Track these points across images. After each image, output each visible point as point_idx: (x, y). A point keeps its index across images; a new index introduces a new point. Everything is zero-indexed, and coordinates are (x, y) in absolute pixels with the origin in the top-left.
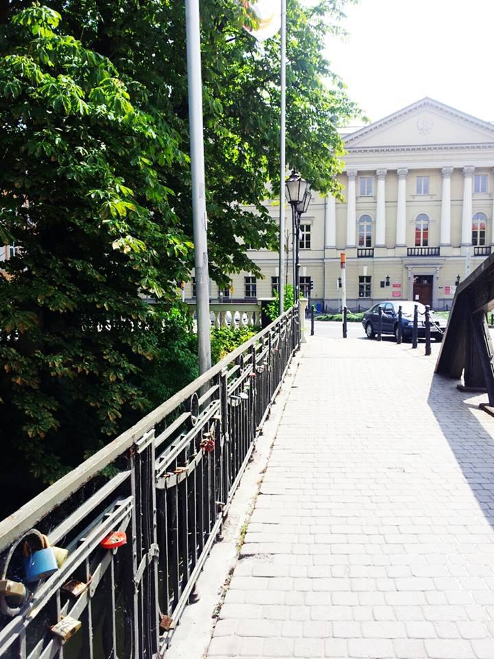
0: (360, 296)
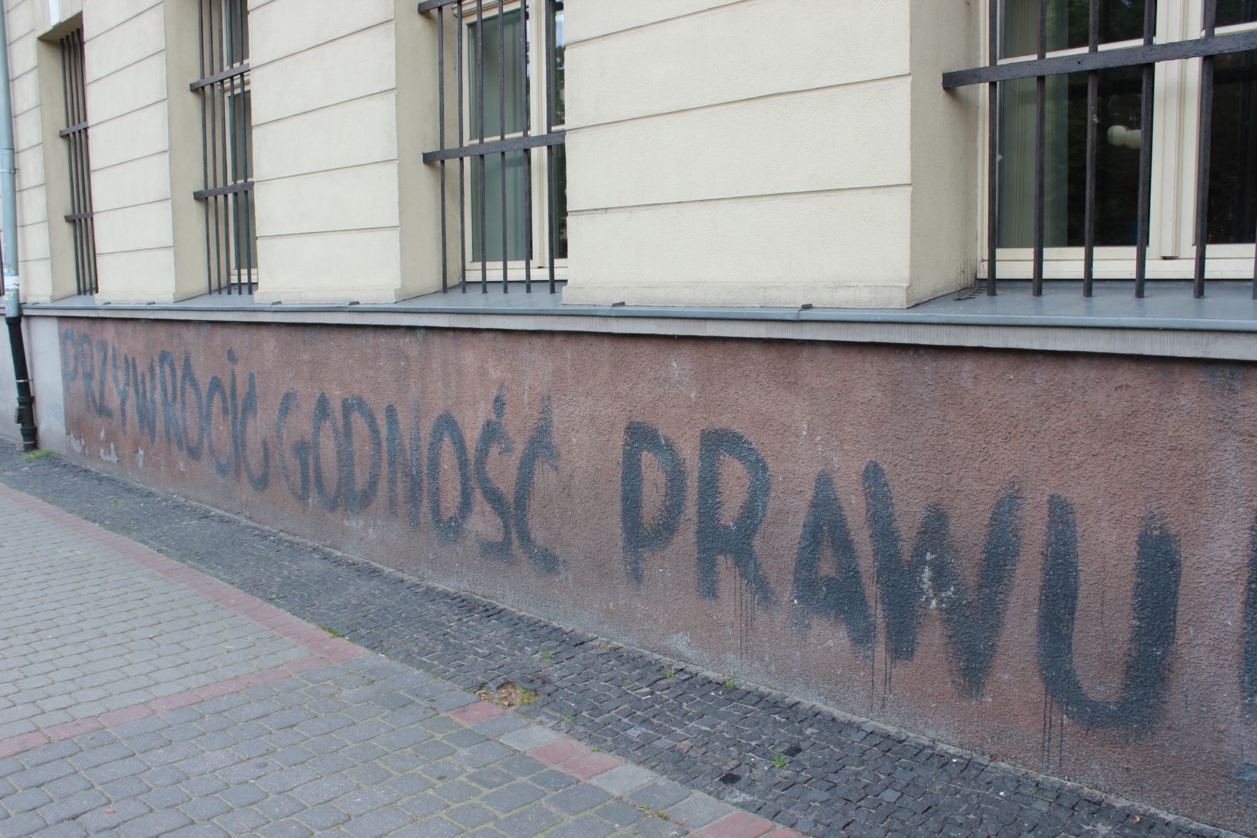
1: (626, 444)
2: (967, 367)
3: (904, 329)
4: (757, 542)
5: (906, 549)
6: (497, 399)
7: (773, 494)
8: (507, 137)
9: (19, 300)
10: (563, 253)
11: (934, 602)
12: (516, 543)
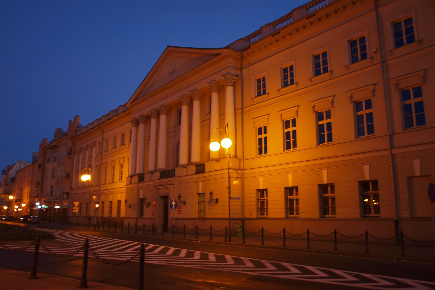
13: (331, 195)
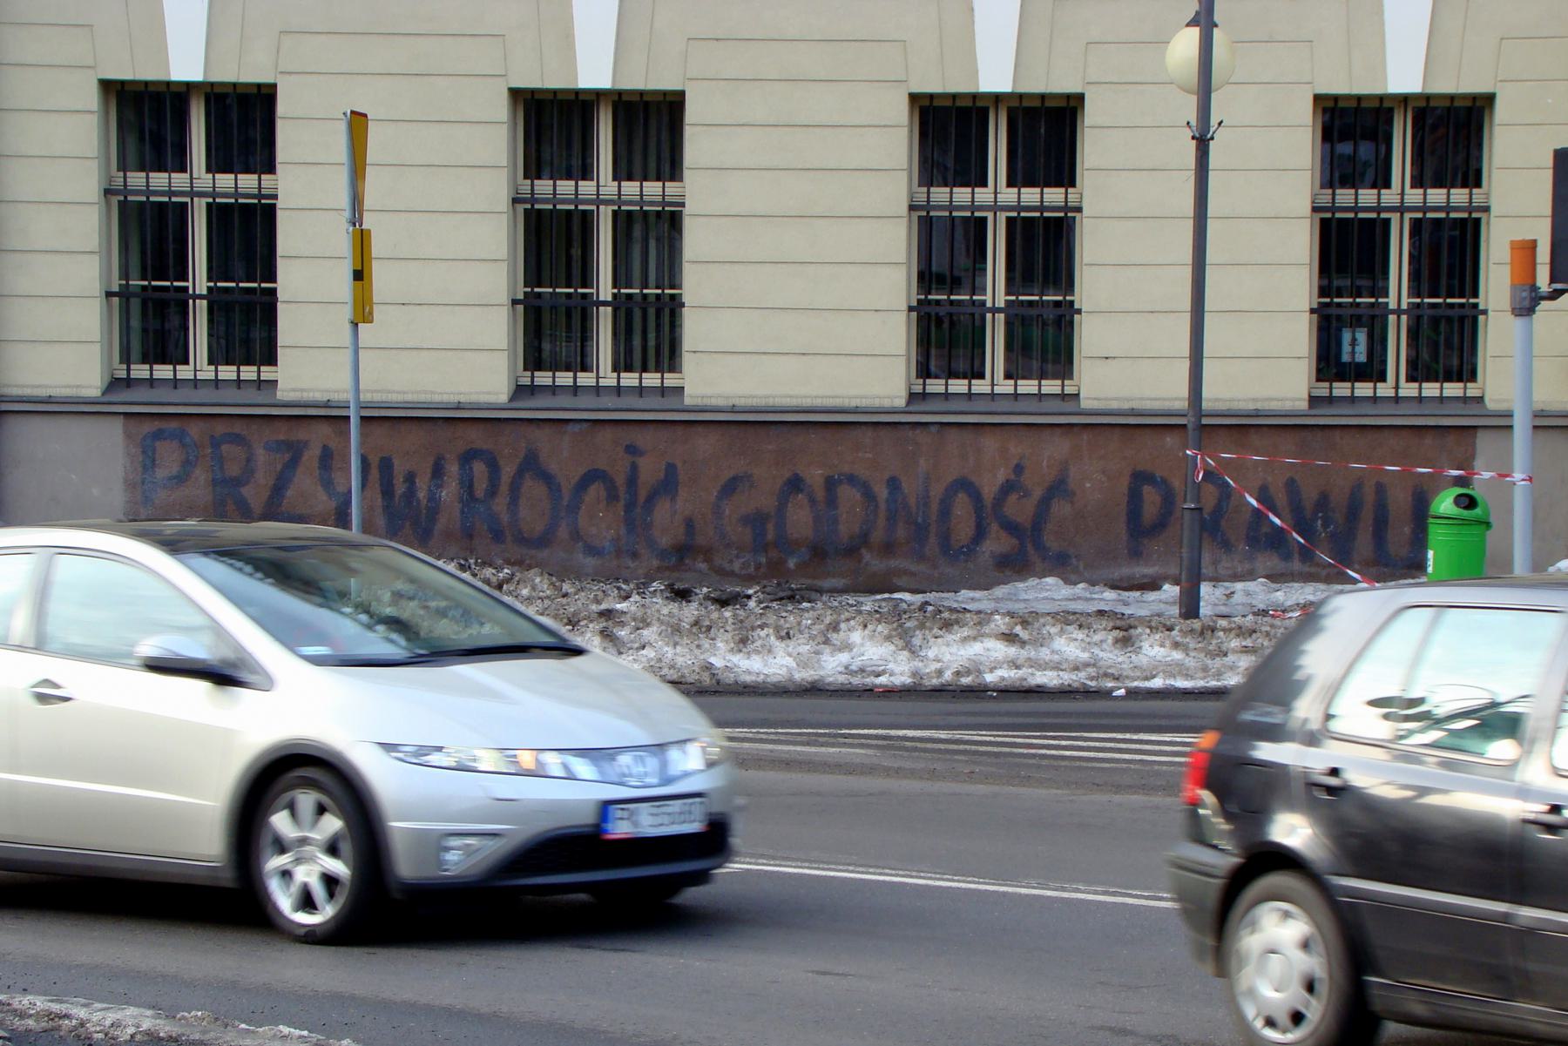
0: (1329, 364)
1: (1130, 483)
2: (1337, 433)
3: (1332, 418)
4: (1223, 523)
5: (1308, 513)
6: (1017, 466)
7: (1233, 498)
8: (638, 208)
9: (359, 398)
10: (368, 318)
11: (1323, 535)
12: (1030, 548)
13: (1414, 196)
